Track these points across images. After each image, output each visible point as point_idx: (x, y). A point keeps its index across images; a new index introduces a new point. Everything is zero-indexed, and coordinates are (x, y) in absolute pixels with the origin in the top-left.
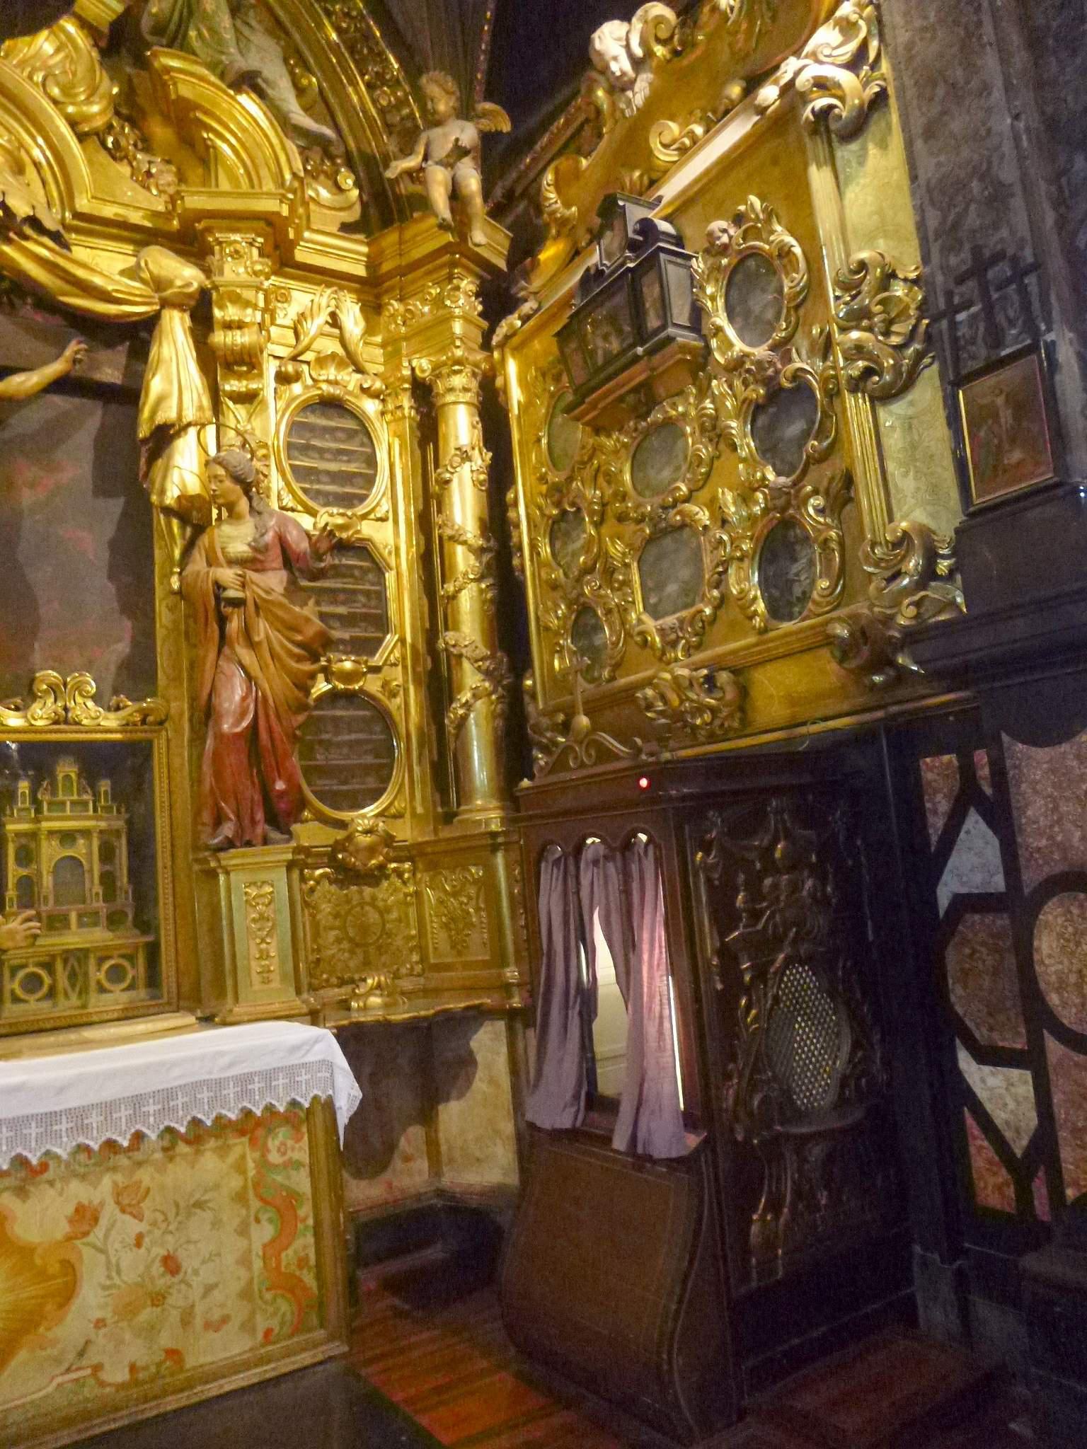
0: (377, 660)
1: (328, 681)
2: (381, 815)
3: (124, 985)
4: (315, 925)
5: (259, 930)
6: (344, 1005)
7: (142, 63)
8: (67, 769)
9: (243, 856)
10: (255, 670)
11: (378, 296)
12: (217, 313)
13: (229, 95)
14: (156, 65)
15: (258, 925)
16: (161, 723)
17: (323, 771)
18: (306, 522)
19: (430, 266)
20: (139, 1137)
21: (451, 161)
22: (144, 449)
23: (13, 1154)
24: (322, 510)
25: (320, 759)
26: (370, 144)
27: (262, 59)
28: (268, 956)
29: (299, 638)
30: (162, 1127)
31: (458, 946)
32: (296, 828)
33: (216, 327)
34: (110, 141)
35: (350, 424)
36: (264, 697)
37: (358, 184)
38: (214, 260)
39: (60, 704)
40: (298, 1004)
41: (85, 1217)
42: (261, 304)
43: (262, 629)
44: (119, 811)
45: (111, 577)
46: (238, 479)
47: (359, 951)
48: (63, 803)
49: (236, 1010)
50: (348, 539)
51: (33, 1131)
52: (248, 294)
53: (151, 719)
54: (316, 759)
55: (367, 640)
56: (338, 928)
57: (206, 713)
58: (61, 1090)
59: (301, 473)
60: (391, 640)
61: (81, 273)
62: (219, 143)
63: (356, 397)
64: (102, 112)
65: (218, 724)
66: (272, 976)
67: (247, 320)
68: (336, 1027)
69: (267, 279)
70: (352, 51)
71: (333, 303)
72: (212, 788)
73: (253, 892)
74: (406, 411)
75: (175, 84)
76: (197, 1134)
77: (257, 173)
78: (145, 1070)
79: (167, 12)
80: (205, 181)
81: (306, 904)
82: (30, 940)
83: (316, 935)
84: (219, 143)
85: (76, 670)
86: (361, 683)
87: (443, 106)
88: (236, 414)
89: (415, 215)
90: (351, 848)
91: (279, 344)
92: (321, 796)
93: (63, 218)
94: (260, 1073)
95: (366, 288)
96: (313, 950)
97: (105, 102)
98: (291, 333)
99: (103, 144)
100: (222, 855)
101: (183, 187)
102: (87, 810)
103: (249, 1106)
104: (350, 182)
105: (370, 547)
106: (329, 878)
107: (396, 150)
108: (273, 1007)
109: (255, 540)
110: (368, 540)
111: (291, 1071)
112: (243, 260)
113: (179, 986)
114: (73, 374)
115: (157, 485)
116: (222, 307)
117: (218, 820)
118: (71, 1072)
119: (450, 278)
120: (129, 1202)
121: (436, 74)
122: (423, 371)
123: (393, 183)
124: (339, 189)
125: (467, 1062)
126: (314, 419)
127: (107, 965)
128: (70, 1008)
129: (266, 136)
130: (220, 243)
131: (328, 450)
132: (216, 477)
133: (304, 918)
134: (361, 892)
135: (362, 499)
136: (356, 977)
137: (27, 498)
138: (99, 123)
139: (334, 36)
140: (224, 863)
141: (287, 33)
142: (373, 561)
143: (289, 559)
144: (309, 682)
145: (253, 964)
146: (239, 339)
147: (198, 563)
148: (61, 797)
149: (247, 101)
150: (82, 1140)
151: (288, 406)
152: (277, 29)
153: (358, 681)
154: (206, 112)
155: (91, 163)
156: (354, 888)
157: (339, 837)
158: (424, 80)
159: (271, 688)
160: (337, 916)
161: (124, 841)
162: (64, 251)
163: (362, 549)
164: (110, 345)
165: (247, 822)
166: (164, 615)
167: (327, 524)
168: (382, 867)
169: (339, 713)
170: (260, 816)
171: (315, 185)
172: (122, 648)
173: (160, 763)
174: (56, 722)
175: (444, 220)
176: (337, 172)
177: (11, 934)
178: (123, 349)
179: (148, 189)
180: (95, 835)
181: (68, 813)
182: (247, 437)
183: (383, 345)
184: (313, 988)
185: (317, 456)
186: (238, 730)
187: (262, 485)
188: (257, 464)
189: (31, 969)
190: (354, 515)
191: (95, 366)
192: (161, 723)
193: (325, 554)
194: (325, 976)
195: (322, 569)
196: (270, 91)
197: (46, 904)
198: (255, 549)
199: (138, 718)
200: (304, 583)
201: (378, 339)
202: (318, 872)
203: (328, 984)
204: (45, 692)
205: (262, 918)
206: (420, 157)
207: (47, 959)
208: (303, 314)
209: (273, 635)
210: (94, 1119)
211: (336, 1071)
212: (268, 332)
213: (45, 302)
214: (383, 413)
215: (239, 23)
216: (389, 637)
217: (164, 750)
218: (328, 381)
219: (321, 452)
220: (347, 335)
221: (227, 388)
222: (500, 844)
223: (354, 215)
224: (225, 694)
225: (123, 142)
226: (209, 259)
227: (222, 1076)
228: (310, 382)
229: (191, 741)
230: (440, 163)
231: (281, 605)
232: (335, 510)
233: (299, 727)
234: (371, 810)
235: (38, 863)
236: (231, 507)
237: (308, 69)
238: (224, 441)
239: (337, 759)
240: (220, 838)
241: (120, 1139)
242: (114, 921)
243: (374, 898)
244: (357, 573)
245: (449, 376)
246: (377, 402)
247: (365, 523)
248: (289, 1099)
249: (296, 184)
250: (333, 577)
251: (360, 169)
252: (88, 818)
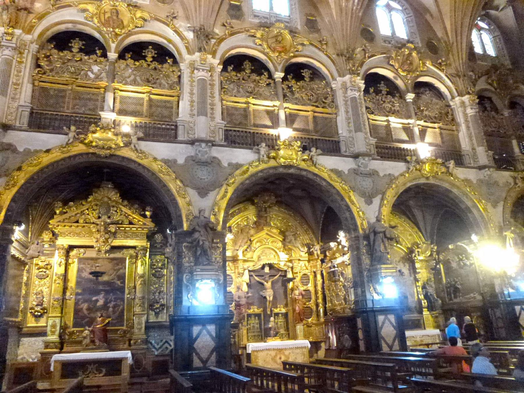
8: (253, 316)
31: (320, 334)
41: (290, 353)
43: (300, 302)
57: (294, 310)
76: (297, 348)
120: (293, 353)
125: (321, 347)
146: (296, 271)
163: (308, 290)
166: (289, 299)
172: (285, 302)
222: (312, 376)
234: (310, 319)
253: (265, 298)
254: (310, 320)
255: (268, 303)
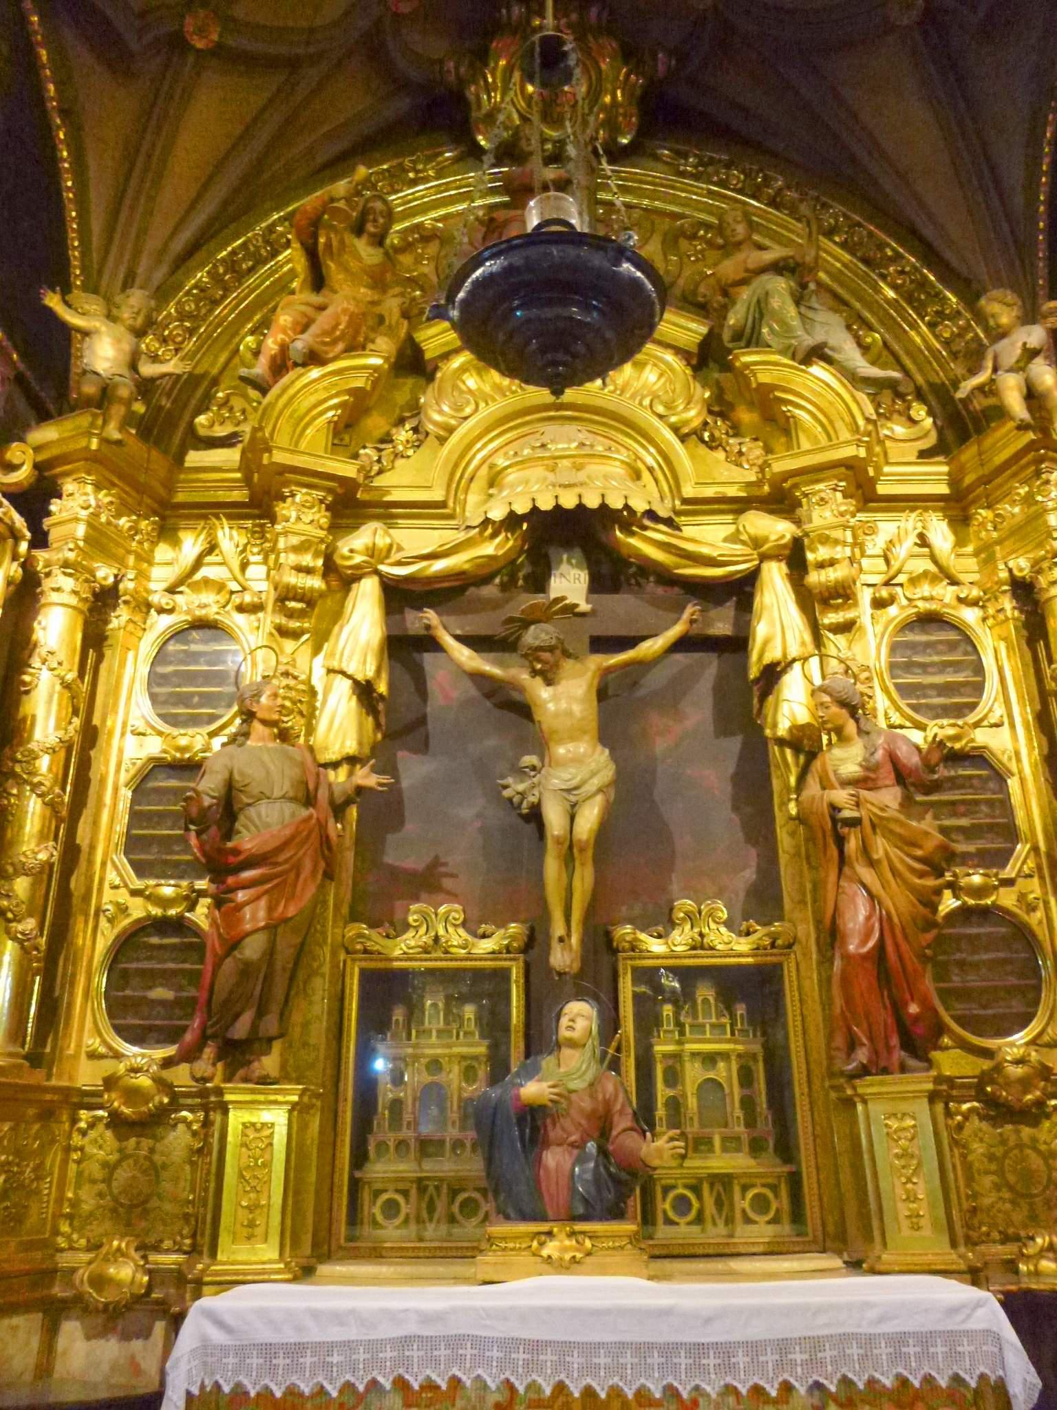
0: (1009, 872)
1: (956, 897)
2: (1033, 1042)
3: (767, 1218)
4: (967, 1167)
5: (904, 1167)
6: (1010, 1266)
7: (727, 367)
8: (705, 992)
9: (881, 1083)
10: (876, 887)
11: (965, 509)
12: (810, 556)
13: (802, 371)
14: (737, 364)
15: (903, 1162)
16: (790, 946)
17: (963, 994)
18: (917, 737)
19: (1014, 468)
20: (787, 1388)
21: (1022, 364)
22: (755, 688)
23: (665, 1382)
24: (931, 723)
25: (956, 980)
26: (938, 374)
27: (827, 332)
28: (916, 1199)
29: (919, 853)
30: (810, 1381)
32: (936, 1055)
33: (810, 568)
34: (706, 435)
35: (953, 636)
36: (888, 914)
37: (930, 413)
38: (801, 512)
39: (696, 930)
40: (952, 1258)
42: (850, 539)
43: (881, 846)
44: (755, 1036)
45: (736, 808)
46: (843, 704)
47: (1023, 1203)
48: (703, 1026)
49: (885, 1257)
50: (962, 749)
51: (683, 1361)
52: (837, 534)
53: (779, 942)
54: (950, 981)
55: (998, 852)
56: (993, 1173)
57: (831, 935)
58: (708, 1321)
59: (904, 690)
60: (1021, 849)
61: (690, 547)
62: (797, 412)
63: (954, 608)
64: (699, 414)
65: (844, 944)
66: (923, 1222)
67: (838, 556)
68: (1002, 1292)
69: (854, 516)
70: (910, 299)
71: (919, 525)
72: (842, 1012)
73: (894, 1124)
74: (1009, 613)
75: (755, 375)
77: (834, 428)
78: (788, 1312)
79: (743, 322)
80: (789, 447)
81: (955, 1143)
82: (679, 1161)
83: (970, 1179)
84: (797, 412)
85: (709, 898)
86: (993, 898)
87: (1005, 317)
88: (837, 643)
89: (993, 425)
90: (1001, 1080)
91: (873, 571)
92: (961, 1021)
93: (674, 506)
94: (914, 1334)
95: (952, 504)
96: (968, 1197)
97: (699, 406)
98: (882, 561)
99: (702, 441)
100: (857, 1082)
101: (770, 456)
102: (725, 1033)
103: (905, 1373)
104: (923, 413)
105: (987, 755)
106: (978, 1114)
107: (964, 372)
108: (925, 1259)
109: (865, 760)
110: (984, 747)
111: (952, 1338)
112: (828, 506)
113: (824, 1225)
114: (691, 633)
115: (769, 720)
116: (813, 550)
117: (852, 1045)
118: (716, 1302)
119: (1038, 474)
121: (995, 293)
122: (1021, 570)
123: (966, 402)
124: (913, 422)
126: (911, 637)
127: (750, 1194)
128: (718, 1236)
129: (838, 395)
130: (806, 495)
131: (932, 664)
132: (822, 704)
133: (953, 1158)
134: (1018, 1132)
135: (973, 707)
136: (1023, 1233)
137: (661, 746)
138: (696, 423)
139: (891, 294)
140: (860, 1091)
141: (846, 303)
142: (992, 768)
143: (901, 775)
144: (934, 898)
145: (900, 1205)
146: (831, 576)
147: (813, 787)
148: (701, 1020)
149: (818, 370)
150: (729, 1380)
151: (886, 628)
152: (839, 303)
153: (987, 896)
154: (785, 390)
155: (693, 457)
156: (1009, 1127)
157: (985, 1067)
158: (983, 302)
159: (894, 904)
160: (991, 1158)
161: (761, 1065)
162: (677, 533)
163: (978, 757)
164: (719, 603)
165: (881, 1046)
166: (785, 840)
167: (935, 736)
168: (1040, 1104)
169: (974, 930)
170: (895, 1041)
171: (889, 424)
172: (749, 875)
173: (791, 986)
174: (693, 948)
175: (1022, 420)
176: (909, 408)
177: (659, 1151)
178: (730, 605)
179: (741, 466)
180: (733, 1058)
181: (708, 1035)
182: (848, 663)
183: (976, 554)
184: (971, 1242)
185: (919, 671)
186: (865, 950)
187: (868, 706)
188: (860, 687)
189: (681, 1191)
190: (966, 724)
191: (709, 624)
192: (790, 946)
193: (937, 765)
194: (984, 1229)
195: (936, 781)
196: (836, 356)
197: (692, 1125)
198: (867, 769)
199: (767, 942)
200: (920, 798)
201: (970, 549)
202: (965, 1107)
203: (987, 1239)
204: (683, 919)
205: (905, 1155)
206: (989, 371)
207: (693, 1181)
208: (891, 541)
209: (895, 853)
210: (741, 1359)
211: (1006, 1347)
212: (860, 564)
213: (667, 578)
214: (984, 619)
215: (803, 310)
216: (1019, 847)
217: (794, 974)
218: (924, 599)
219: (924, 667)
220: (937, 552)
221: (826, 621)
223: (932, 440)
224: (848, 915)
225: (717, 434)
226: (799, 511)
227: (872, 1331)
228: (905, 602)
229: (820, 963)
230: (1010, 370)
231: (897, 821)
232: (945, 722)
233: (928, 946)
234: (1021, 1037)
235: (683, 1085)
236: (839, 731)
237: (871, 328)
238: (829, 670)
239: (973, 981)
240: (854, 1064)
241: (767, 1387)
242: (756, 1147)
243: (1034, 1140)
244: (975, 782)
245: (1050, 569)
246: (976, 609)
247: (978, 730)
248: (950, 1372)
249: (870, 427)
250: (950, 789)
251: (931, 398)
252: (728, 1041)
253: (535, 816)
254: (1016, 1043)
255: (552, 867)
